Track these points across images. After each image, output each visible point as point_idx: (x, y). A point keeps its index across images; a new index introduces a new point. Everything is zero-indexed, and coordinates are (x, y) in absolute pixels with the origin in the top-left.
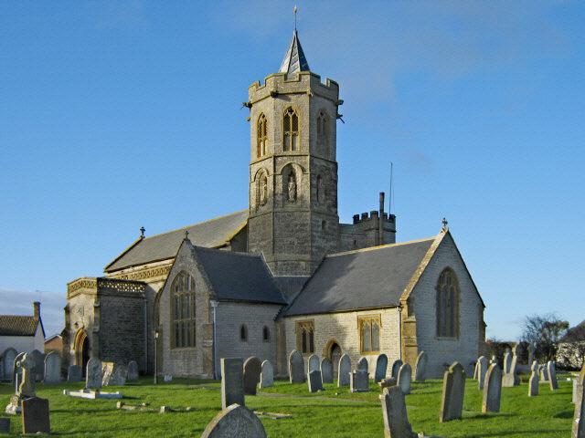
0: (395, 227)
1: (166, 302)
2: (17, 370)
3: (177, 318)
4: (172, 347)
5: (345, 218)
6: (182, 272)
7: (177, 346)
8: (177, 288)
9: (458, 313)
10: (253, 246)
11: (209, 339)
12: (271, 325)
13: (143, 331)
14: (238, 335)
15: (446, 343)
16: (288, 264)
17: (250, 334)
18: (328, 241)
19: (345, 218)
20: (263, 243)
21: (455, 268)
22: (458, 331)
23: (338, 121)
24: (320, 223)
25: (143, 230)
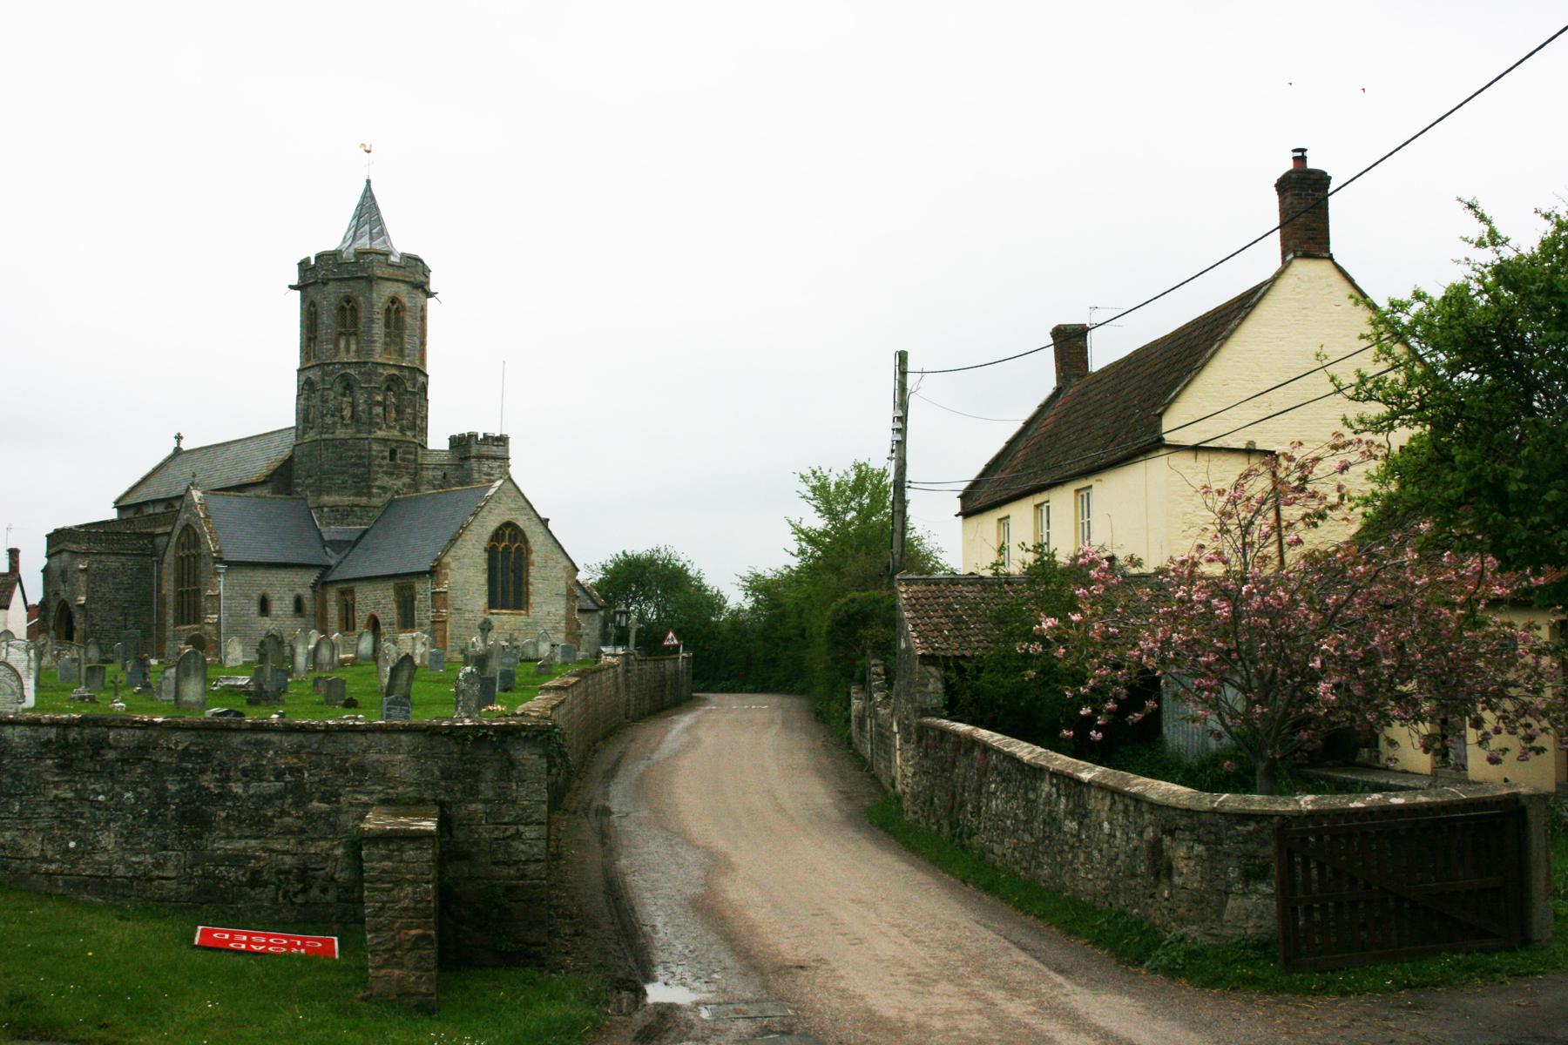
0: (507, 452)
1: (169, 564)
2: (129, 865)
3: (183, 586)
4: (176, 624)
5: (438, 440)
6: (188, 525)
7: (347, 630)
8: (183, 545)
9: (528, 580)
10: (298, 485)
11: (213, 613)
12: (307, 594)
13: (152, 602)
14: (255, 609)
15: (505, 620)
16: (338, 511)
17: (275, 607)
18: (399, 477)
19: (438, 440)
20: (310, 481)
21: (522, 522)
22: (527, 602)
23: (430, 301)
24: (387, 454)
25: (179, 438)
